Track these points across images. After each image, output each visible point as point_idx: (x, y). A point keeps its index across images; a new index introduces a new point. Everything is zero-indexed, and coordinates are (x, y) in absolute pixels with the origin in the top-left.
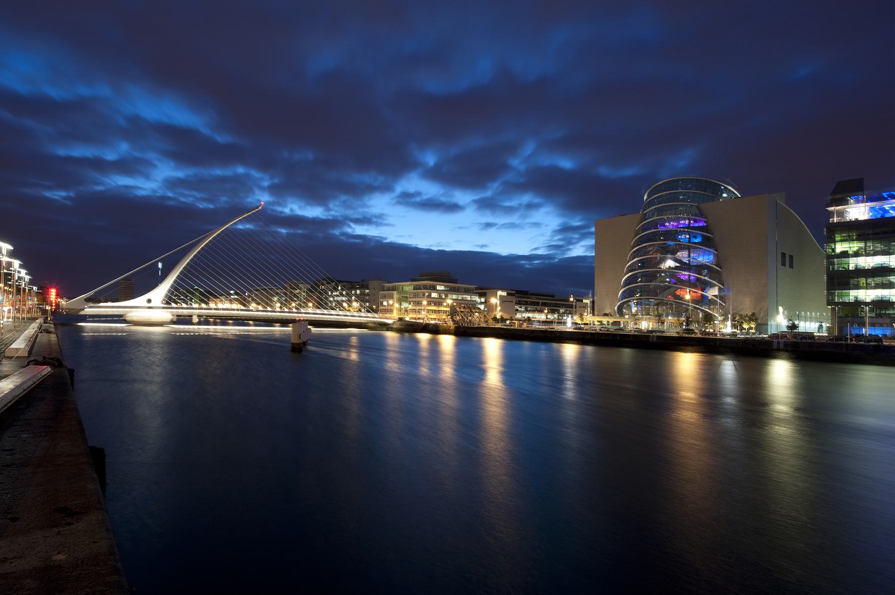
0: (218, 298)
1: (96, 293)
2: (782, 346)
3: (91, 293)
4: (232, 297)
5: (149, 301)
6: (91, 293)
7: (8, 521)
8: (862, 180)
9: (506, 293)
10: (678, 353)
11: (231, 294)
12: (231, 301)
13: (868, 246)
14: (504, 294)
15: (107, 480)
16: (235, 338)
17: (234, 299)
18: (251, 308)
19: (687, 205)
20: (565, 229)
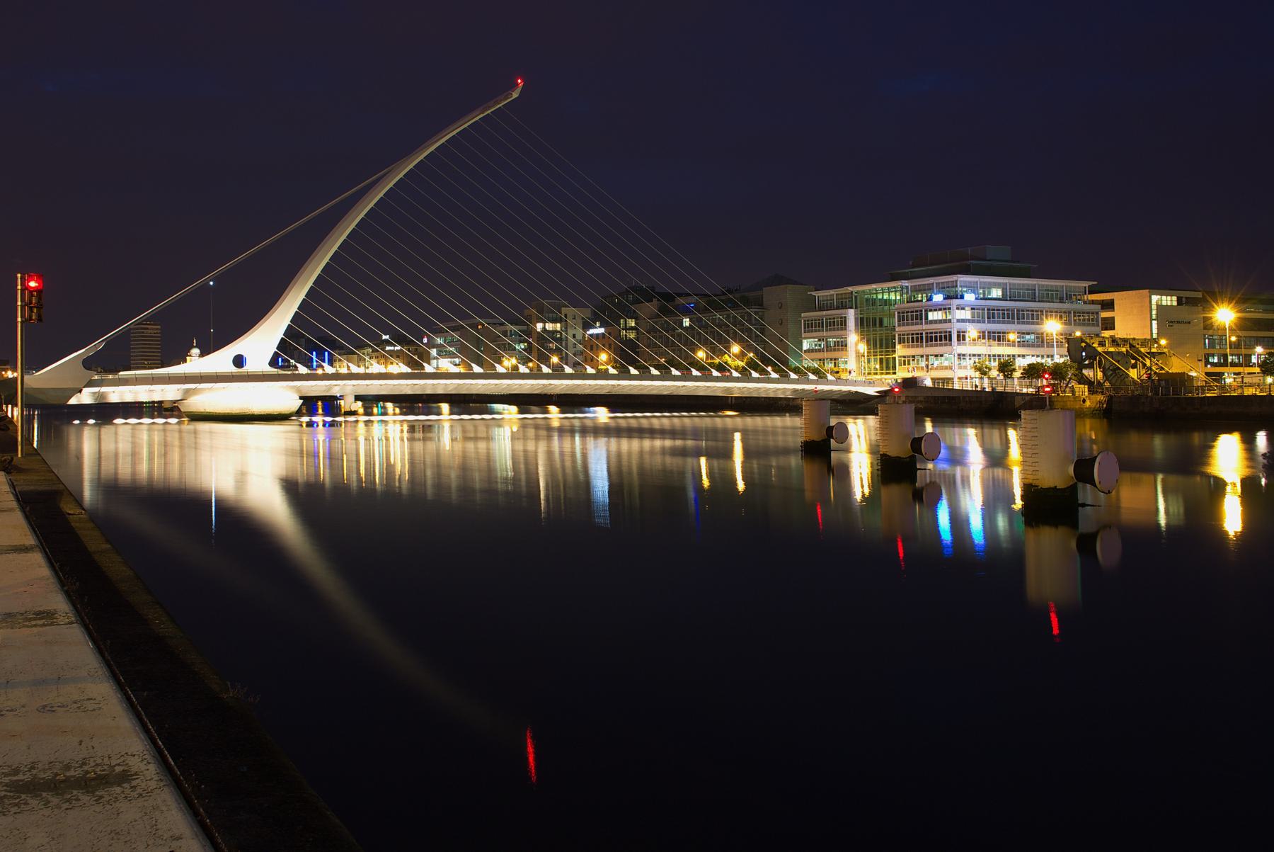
0: (354, 353)
1: (109, 343)
2: (968, 358)
3: (98, 344)
4: (388, 348)
5: (239, 361)
6: (98, 344)
7: (854, 349)
8: (1113, 300)
9: (1175, 298)
10: (974, 537)
11: (387, 343)
12: (383, 358)
13: (384, 408)
14: (1169, 300)
15: (72, 524)
16: (73, 460)
17: (391, 353)
18: (500, 369)
19: (895, 339)
20: (37, 546)
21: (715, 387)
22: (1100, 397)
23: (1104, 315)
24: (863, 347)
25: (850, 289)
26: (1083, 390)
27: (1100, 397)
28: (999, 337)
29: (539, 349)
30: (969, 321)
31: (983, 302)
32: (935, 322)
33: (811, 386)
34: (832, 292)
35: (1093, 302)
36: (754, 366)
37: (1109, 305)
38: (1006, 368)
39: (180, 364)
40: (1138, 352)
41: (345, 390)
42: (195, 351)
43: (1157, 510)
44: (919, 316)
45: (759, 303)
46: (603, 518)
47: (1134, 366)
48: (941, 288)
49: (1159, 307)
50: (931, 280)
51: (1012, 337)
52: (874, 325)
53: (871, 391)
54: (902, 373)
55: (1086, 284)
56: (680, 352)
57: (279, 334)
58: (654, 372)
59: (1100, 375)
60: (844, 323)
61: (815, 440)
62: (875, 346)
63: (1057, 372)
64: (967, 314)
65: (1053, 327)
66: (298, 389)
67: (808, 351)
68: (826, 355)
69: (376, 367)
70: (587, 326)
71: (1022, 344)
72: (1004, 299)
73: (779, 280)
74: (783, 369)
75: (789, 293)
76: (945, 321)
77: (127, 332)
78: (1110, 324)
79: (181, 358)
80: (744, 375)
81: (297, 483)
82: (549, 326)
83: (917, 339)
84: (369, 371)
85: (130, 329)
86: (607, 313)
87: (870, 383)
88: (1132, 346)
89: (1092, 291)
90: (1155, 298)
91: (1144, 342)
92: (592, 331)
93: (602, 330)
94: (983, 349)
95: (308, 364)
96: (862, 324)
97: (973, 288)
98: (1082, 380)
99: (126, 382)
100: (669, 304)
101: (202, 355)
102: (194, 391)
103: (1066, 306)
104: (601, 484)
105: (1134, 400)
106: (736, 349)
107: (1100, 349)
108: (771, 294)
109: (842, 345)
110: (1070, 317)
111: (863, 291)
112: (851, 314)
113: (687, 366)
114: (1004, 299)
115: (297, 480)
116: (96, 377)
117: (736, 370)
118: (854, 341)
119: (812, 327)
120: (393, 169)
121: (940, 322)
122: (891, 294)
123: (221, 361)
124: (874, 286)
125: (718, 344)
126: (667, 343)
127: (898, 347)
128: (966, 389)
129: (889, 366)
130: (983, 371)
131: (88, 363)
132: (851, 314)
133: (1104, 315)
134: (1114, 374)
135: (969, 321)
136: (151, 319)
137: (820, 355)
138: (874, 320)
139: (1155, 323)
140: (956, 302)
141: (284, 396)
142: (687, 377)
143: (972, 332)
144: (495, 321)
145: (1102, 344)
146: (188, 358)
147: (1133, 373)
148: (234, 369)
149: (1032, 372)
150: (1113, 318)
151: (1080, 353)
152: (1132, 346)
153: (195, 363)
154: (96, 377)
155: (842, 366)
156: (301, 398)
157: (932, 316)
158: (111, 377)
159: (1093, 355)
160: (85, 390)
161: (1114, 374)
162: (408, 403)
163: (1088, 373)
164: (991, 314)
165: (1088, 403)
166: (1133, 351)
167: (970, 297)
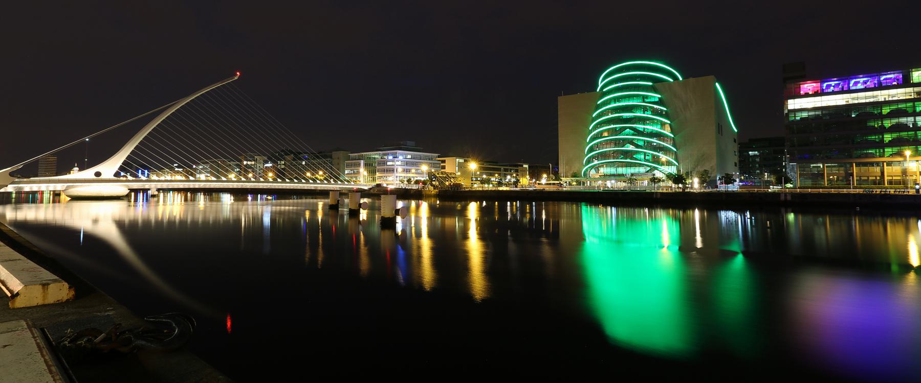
1: (25, 166)
3: (19, 166)
5: (98, 174)
6: (19, 166)
21: (311, 186)
22: (437, 190)
23: (442, 164)
24: (365, 173)
25: (362, 153)
26: (431, 188)
27: (437, 190)
28: (408, 171)
29: (244, 171)
30: (400, 165)
31: (405, 160)
32: (389, 165)
33: (347, 186)
34: (356, 154)
35: (439, 160)
36: (325, 179)
37: (444, 162)
38: (409, 181)
39: (67, 174)
40: (449, 177)
41: (153, 187)
42: (76, 169)
43: (456, 226)
44: (384, 163)
45: (331, 157)
46: (267, 232)
47: (447, 181)
48: (392, 154)
49: (458, 162)
50: (389, 152)
51: (413, 171)
52: (370, 166)
53: (366, 188)
54: (378, 182)
55: (437, 155)
56: (299, 174)
57: (120, 163)
58: (287, 180)
59: (437, 183)
60: (359, 165)
61: (334, 204)
62: (370, 173)
63: (424, 183)
64: (399, 163)
65: (425, 168)
66: (127, 186)
67: (347, 174)
68: (353, 175)
69: (169, 178)
70: (267, 162)
71: (416, 173)
72: (411, 159)
73: (338, 149)
74: (337, 178)
75: (341, 154)
76: (392, 165)
77: (37, 161)
78: (444, 167)
79: (68, 171)
80: (275, 181)
81: (125, 224)
82: (249, 163)
83: (383, 171)
84: (166, 179)
85: (39, 160)
86: (273, 159)
87: (365, 185)
88: (447, 175)
89: (439, 157)
90: (457, 160)
91: (451, 174)
92: (266, 165)
93: (271, 165)
94: (403, 175)
95: (226, 176)
96: (366, 165)
97: (402, 155)
98: (432, 185)
99: (34, 182)
100: (298, 156)
101: (80, 170)
102: (73, 187)
103: (431, 161)
104: (267, 220)
105: (446, 191)
106: (321, 173)
107: (437, 176)
108: (335, 154)
109: (358, 173)
110: (432, 165)
111: (367, 155)
112: (362, 162)
113: (300, 178)
114: (411, 159)
115: (124, 221)
116: (17, 180)
117: (311, 179)
118: (363, 171)
119: (349, 166)
120: (786, 219)
121: (391, 165)
122: (376, 155)
123: (89, 173)
124: (370, 153)
125: (315, 172)
126: (294, 171)
127: (377, 173)
128: (667, 191)
129: (374, 180)
130: (402, 182)
131: (12, 174)
132: (362, 162)
133: (442, 164)
134: (441, 183)
135: (400, 165)
136: (53, 155)
137: (351, 175)
138: (370, 164)
139: (457, 168)
140: (396, 159)
141: (120, 189)
142: (300, 182)
143: (400, 169)
144: (221, 160)
145: (438, 174)
146: (71, 172)
147: (447, 183)
148: (95, 177)
149: (417, 182)
150: (445, 166)
151: (431, 176)
152: (447, 175)
153: (75, 174)
154: (17, 180)
155: (358, 179)
156: (129, 189)
157: (388, 163)
158: (25, 180)
159: (435, 177)
160: (9, 186)
161: (441, 183)
162: (185, 190)
163: (434, 183)
164: (407, 164)
165: (433, 192)
166: (448, 177)
167: (401, 158)
